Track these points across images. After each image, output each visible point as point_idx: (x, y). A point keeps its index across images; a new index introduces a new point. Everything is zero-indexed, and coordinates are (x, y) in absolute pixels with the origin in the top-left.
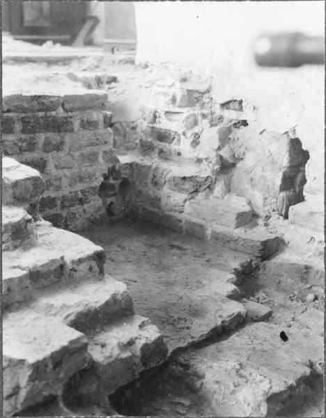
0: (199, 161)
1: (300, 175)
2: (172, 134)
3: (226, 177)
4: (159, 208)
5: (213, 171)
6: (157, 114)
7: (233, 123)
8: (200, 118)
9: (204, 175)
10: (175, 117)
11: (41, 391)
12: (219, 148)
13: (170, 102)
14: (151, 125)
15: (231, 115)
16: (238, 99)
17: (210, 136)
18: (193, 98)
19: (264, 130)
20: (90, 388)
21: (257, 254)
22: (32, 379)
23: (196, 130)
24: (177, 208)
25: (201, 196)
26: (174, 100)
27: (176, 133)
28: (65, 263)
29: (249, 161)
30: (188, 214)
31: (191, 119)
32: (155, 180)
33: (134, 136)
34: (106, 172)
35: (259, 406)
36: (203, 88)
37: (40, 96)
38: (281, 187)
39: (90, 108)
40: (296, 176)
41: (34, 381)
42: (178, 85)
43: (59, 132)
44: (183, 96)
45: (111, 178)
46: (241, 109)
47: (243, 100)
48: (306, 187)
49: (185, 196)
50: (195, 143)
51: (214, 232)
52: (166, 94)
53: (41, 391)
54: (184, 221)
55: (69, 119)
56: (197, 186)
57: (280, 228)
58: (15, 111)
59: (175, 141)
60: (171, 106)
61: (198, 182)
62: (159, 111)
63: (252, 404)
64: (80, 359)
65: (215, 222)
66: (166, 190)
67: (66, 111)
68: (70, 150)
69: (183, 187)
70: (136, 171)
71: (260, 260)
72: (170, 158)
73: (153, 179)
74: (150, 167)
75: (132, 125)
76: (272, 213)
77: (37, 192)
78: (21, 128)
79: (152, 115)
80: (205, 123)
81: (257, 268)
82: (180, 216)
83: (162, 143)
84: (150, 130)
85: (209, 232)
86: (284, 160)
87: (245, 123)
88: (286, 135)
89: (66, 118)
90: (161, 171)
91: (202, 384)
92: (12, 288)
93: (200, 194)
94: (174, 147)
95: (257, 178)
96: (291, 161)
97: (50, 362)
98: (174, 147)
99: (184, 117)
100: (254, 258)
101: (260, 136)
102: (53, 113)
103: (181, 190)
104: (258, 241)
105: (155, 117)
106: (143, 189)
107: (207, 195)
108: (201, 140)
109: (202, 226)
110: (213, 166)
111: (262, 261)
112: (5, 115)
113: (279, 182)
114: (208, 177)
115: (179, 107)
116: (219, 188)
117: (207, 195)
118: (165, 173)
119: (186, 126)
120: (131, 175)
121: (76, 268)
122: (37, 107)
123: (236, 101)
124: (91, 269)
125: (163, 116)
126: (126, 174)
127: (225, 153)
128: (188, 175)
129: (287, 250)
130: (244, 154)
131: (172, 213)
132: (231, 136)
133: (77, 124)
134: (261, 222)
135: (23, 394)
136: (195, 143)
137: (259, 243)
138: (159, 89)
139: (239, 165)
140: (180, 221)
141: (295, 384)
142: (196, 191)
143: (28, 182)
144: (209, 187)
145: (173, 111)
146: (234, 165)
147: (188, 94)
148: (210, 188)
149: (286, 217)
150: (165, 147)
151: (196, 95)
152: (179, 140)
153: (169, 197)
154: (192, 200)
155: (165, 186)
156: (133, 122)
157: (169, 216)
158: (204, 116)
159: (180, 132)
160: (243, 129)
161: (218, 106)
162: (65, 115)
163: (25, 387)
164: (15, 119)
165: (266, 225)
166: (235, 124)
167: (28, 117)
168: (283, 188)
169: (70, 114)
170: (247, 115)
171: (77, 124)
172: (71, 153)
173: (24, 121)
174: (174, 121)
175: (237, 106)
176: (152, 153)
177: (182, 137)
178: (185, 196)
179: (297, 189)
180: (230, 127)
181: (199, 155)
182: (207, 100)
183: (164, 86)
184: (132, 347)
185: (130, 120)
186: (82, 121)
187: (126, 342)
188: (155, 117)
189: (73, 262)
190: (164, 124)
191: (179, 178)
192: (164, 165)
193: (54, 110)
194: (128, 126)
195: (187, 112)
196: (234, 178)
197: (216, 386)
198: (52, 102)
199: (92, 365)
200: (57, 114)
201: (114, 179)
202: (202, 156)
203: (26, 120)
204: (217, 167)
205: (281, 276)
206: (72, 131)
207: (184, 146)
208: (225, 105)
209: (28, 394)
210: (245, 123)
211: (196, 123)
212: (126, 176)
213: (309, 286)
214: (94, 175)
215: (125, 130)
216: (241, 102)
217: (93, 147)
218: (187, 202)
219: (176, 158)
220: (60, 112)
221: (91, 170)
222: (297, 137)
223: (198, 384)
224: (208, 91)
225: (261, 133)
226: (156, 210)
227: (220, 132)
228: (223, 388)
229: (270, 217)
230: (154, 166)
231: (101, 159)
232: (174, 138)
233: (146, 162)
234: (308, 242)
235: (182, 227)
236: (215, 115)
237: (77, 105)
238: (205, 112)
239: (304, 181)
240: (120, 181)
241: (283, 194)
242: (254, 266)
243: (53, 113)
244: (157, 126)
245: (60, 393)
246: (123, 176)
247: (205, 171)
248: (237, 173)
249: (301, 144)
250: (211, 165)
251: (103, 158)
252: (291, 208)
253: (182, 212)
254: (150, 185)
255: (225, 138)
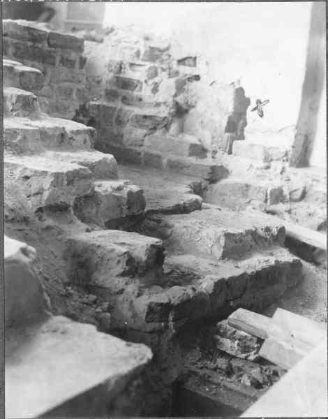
0: (158, 105)
1: (241, 122)
2: (135, 82)
3: (180, 120)
4: (121, 144)
5: (169, 113)
6: (123, 66)
7: (186, 77)
8: (159, 70)
9: (163, 115)
10: (137, 68)
11: (59, 197)
12: (176, 95)
13: (135, 55)
14: (117, 75)
15: (186, 70)
16: (194, 56)
17: (167, 85)
18: (154, 54)
19: (214, 82)
20: (91, 211)
21: (205, 177)
22: (54, 185)
23: (156, 80)
24: (138, 143)
25: (158, 133)
26: (138, 54)
27: (139, 81)
28: (65, 132)
29: (200, 108)
30: (148, 147)
31: (152, 71)
32: (120, 119)
33: (98, 89)
34: (78, 108)
35: (219, 239)
36: (163, 46)
37: (31, 28)
38: (226, 129)
39: (72, 48)
40: (238, 121)
41: (55, 186)
42: (142, 42)
43: (43, 62)
44: (146, 52)
45: (81, 115)
46: (195, 65)
47: (198, 56)
48: (246, 129)
49: (145, 131)
50: (155, 90)
51: (169, 161)
52: (132, 49)
53: (59, 197)
54: (143, 154)
55: (52, 54)
56: (155, 124)
57: (224, 159)
58: (10, 37)
59: (138, 88)
60: (136, 58)
61: (156, 121)
62: (125, 62)
63: (213, 237)
64: (87, 183)
65: (170, 152)
66: (128, 127)
67: (50, 45)
68: (50, 81)
69: (144, 124)
70: (102, 113)
71: (208, 182)
72: (131, 103)
73: (117, 119)
74: (115, 108)
75: (97, 79)
76: (218, 150)
77: (37, 86)
78: (14, 51)
79: (118, 66)
80: (165, 74)
81: (205, 189)
82: (138, 149)
83: (127, 91)
84: (115, 79)
85: (165, 161)
86: (229, 106)
87: (197, 78)
88: (232, 86)
89: (50, 52)
90: (124, 112)
91: (172, 231)
92: (28, 137)
93: (158, 131)
94: (136, 93)
95: (206, 121)
96: (235, 108)
97: (65, 178)
98: (136, 93)
99: (147, 68)
100: (203, 181)
101: (211, 88)
102: (40, 45)
103: (142, 126)
104: (207, 166)
105: (121, 68)
106: (107, 127)
107: (164, 133)
108: (160, 88)
109: (159, 157)
110: (170, 109)
111: (210, 184)
112: (5, 38)
113: (224, 124)
114: (165, 117)
115: (143, 60)
116: (174, 127)
117: (164, 133)
118: (128, 113)
119: (147, 76)
120: (98, 116)
121: (75, 137)
122: (28, 36)
123: (190, 58)
124: (85, 142)
125: (127, 66)
126: (94, 114)
127: (180, 99)
128: (148, 114)
129: (230, 177)
130: (196, 102)
131: (131, 148)
132: (185, 87)
133: (58, 59)
134: (209, 155)
135: (46, 194)
136: (155, 90)
137: (208, 168)
138: (126, 45)
139: (192, 111)
140: (140, 154)
141: (244, 233)
142: (155, 129)
143: (31, 74)
144: (165, 126)
145: (137, 63)
146: (187, 111)
147: (150, 51)
148: (167, 127)
149: (230, 153)
150: (128, 93)
151: (157, 53)
152: (141, 88)
153: (131, 133)
154: (151, 136)
155: (128, 124)
156: (98, 77)
157: (131, 150)
158: (163, 70)
159: (142, 80)
160: (195, 83)
161: (175, 63)
162: (49, 49)
163: (49, 189)
164: (9, 42)
165: (213, 157)
166: (189, 78)
167: (20, 44)
168: (227, 130)
169: (53, 49)
170: (200, 69)
171: (58, 59)
172: (52, 84)
173: (17, 47)
174: (138, 71)
175: (191, 62)
176: (116, 100)
177: (144, 85)
178: (145, 131)
179: (239, 133)
180: (185, 80)
181: (157, 100)
182: (167, 57)
183: (129, 42)
184: (122, 192)
185: (96, 75)
186: (62, 58)
187: (116, 187)
188: (121, 68)
189: (72, 132)
190: (129, 74)
191: (140, 116)
192: (127, 108)
193: (40, 43)
194: (94, 80)
195: (149, 64)
196: (187, 121)
197: (185, 230)
198: (40, 35)
199: (93, 195)
200: (43, 46)
201: (83, 116)
202: (161, 100)
203: (18, 45)
204: (173, 110)
205: (226, 195)
206: (53, 64)
207: (145, 92)
208: (181, 62)
209: (51, 195)
210: (197, 78)
211: (156, 74)
212: (94, 116)
213: (248, 200)
214: (68, 109)
215: (90, 83)
216: (195, 58)
217: (72, 84)
218: (147, 137)
219: (138, 103)
220: (45, 46)
221: (66, 103)
222: (241, 86)
223: (169, 231)
224: (168, 49)
225: (211, 84)
226: (118, 145)
227: (177, 81)
228: (190, 230)
229: (216, 152)
230: (119, 107)
231: (74, 96)
232: (137, 86)
233: (111, 104)
234: (248, 170)
235: (140, 159)
236: (172, 71)
237: (59, 43)
238: (165, 66)
239: (245, 124)
240: (89, 119)
241: (227, 134)
242: (203, 187)
243: (40, 45)
244: (121, 75)
245: (72, 203)
246: (91, 115)
247: (164, 112)
248: (190, 119)
249: (244, 93)
250: (168, 108)
251: (76, 95)
252: (235, 142)
253: (141, 145)
254: (114, 124)
255: (180, 87)
